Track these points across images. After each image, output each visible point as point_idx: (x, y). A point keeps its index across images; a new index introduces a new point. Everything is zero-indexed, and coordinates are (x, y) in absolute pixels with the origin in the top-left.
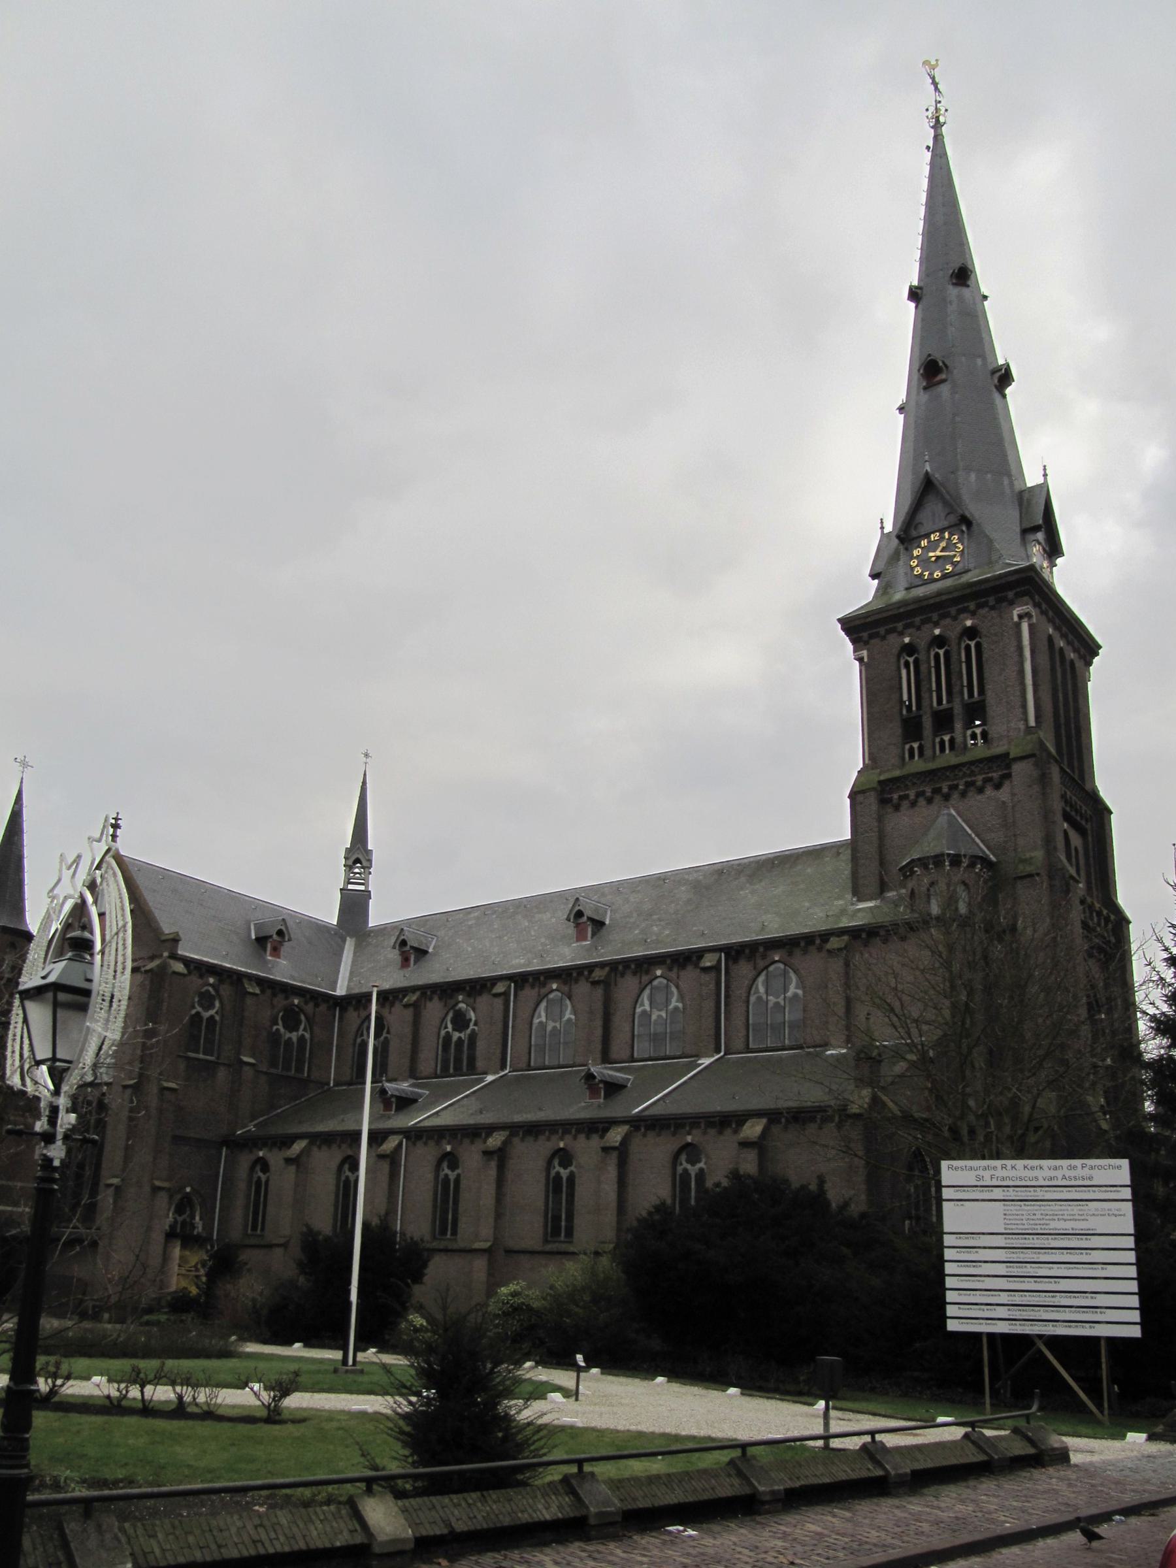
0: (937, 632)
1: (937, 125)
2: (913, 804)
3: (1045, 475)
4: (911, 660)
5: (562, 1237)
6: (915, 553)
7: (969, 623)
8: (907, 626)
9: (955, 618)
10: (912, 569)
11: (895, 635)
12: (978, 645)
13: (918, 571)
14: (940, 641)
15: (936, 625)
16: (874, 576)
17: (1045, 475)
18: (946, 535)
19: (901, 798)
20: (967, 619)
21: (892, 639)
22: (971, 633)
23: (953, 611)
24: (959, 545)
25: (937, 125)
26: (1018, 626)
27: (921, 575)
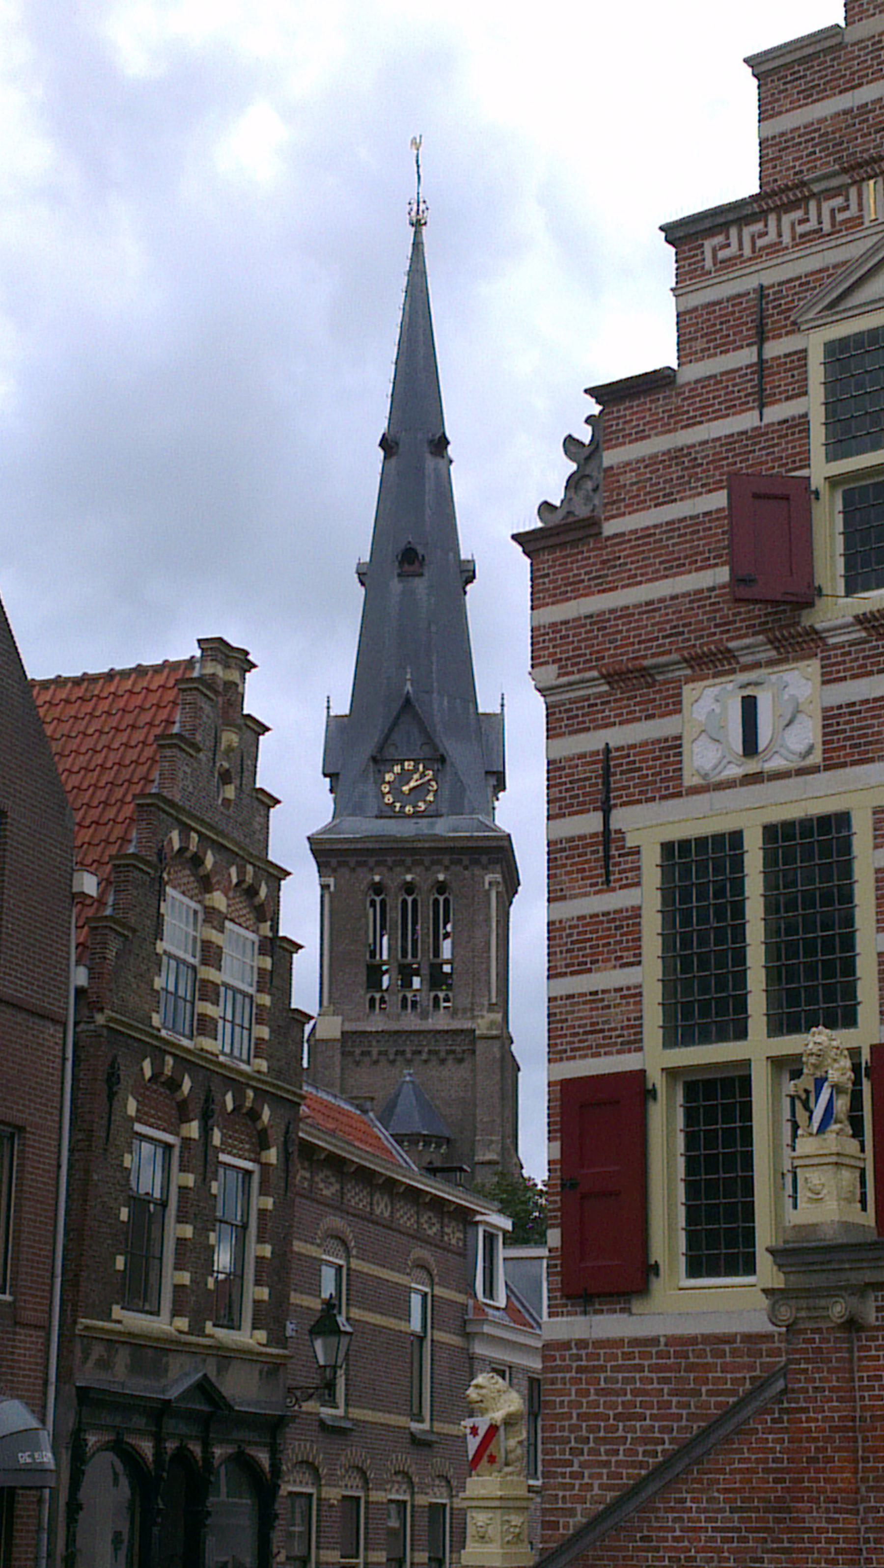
0: (409, 877)
1: (418, 225)
2: (443, 1061)
3: (502, 705)
4: (378, 899)
5: (782, 899)
6: (389, 777)
7: (441, 877)
8: (378, 864)
9: (427, 869)
10: (383, 795)
11: (365, 869)
12: (446, 901)
13: (389, 799)
14: (409, 888)
15: (409, 870)
16: (325, 775)
17: (502, 705)
18: (421, 767)
19: (363, 1054)
20: (438, 872)
21: (362, 872)
22: (442, 888)
23: (427, 860)
24: (433, 783)
25: (418, 225)
26: (487, 893)
27: (392, 806)
